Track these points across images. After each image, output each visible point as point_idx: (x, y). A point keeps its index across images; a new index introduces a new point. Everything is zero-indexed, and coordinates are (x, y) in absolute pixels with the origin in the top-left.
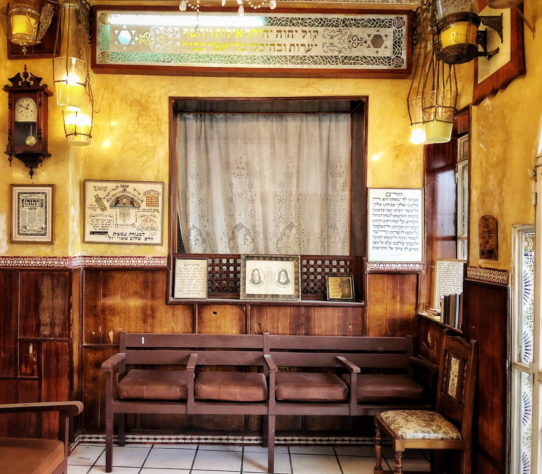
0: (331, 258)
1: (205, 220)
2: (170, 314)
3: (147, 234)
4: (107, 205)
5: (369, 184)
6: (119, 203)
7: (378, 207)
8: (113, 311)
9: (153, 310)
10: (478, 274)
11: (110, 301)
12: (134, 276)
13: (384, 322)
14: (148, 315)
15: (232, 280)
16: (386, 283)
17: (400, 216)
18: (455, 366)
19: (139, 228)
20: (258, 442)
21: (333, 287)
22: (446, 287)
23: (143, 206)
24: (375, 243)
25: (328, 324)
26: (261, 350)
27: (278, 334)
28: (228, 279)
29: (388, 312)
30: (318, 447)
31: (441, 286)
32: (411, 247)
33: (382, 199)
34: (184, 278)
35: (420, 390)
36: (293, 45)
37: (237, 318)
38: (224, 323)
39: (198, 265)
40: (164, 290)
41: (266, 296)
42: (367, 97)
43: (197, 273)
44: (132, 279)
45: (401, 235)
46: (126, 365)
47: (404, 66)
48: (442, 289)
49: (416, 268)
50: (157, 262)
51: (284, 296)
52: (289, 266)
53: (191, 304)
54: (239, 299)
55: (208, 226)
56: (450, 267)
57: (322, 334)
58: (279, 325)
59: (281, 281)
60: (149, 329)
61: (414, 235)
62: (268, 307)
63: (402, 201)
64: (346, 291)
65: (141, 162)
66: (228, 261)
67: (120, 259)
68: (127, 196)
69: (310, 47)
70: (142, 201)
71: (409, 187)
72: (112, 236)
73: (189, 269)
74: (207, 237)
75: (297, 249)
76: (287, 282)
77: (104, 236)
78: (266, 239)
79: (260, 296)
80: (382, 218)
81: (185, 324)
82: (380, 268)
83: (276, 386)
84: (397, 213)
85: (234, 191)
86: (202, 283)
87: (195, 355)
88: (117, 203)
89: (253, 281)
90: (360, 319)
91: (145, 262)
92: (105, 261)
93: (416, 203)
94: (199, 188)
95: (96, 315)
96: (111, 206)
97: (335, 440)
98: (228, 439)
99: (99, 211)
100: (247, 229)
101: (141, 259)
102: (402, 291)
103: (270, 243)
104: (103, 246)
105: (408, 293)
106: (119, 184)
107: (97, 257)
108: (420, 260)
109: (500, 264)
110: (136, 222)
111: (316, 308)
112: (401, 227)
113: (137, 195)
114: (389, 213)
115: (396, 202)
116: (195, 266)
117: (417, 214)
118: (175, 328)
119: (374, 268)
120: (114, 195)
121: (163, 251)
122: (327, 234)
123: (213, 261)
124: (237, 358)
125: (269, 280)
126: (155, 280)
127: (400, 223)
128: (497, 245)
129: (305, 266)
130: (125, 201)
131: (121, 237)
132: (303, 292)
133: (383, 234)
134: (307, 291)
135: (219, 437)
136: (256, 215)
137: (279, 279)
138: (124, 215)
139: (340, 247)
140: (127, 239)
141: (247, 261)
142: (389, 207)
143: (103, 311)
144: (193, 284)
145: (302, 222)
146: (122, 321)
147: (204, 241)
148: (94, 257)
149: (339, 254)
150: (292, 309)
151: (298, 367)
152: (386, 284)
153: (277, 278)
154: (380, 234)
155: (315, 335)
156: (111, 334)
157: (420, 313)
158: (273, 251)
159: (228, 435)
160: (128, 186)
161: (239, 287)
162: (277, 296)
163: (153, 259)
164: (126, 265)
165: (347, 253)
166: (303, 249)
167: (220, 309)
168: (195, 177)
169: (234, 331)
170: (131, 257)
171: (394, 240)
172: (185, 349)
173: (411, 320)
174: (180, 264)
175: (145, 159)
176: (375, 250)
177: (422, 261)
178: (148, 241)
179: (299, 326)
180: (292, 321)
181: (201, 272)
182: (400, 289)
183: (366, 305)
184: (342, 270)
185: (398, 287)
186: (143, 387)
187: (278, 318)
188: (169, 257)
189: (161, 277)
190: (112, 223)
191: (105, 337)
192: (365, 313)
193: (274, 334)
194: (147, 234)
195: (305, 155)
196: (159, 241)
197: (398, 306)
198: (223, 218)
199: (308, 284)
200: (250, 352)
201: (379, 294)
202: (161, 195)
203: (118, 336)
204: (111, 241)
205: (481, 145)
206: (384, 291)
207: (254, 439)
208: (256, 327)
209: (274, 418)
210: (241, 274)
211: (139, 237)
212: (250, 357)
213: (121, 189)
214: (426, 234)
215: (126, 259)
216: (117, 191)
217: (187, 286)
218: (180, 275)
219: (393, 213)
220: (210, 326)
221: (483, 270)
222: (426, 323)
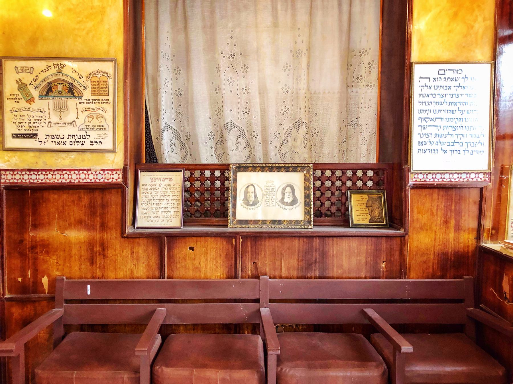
1: (184, 117)
2: (127, 252)
3: (94, 136)
4: (35, 94)
5: (414, 56)
6: (52, 91)
7: (426, 91)
8: (46, 247)
9: (104, 246)
11: (42, 234)
12: (76, 196)
13: (432, 257)
14: (96, 252)
15: (217, 200)
16: (436, 201)
19: (82, 127)
23: (87, 94)
24: (421, 143)
25: (350, 259)
26: (257, 301)
27: (281, 277)
28: (212, 200)
29: (437, 244)
32: (474, 149)
33: (432, 80)
34: (150, 198)
35: (501, 373)
37: (224, 255)
38: (205, 262)
39: (171, 180)
40: (119, 217)
41: (264, 222)
43: (169, 191)
44: (73, 202)
46: (64, 325)
50: (108, 176)
51: (290, 222)
52: (297, 179)
53: (156, 237)
54: (226, 226)
55: (188, 125)
57: (344, 276)
58: (283, 265)
60: (99, 273)
62: (267, 239)
63: (461, 81)
64: (377, 213)
65: (84, 30)
66: (212, 174)
67: (56, 172)
68: (64, 80)
70: (85, 88)
72: (43, 140)
73: (157, 186)
74: (186, 140)
75: (306, 156)
76: (294, 202)
77: (32, 140)
78: (265, 142)
79: (256, 222)
80: (432, 107)
81: (149, 265)
82: (428, 180)
83: (278, 365)
84: (454, 99)
85: (222, 76)
86: (176, 206)
87: (162, 310)
88: (49, 91)
90: (397, 253)
91: (91, 177)
92: (34, 177)
94: (176, 74)
95: (23, 255)
96: (41, 97)
99: (23, 103)
100: (240, 130)
101: (85, 172)
102: (458, 213)
103: (271, 147)
104: (31, 154)
105: (467, 215)
106: (51, 63)
107: (22, 171)
108: (486, 168)
110: (77, 118)
111: (335, 239)
112: (459, 119)
113: (77, 78)
114: (442, 100)
115: (454, 83)
116: (166, 182)
118: (135, 272)
119: (418, 180)
120: (44, 80)
121: (117, 160)
122: (347, 135)
123: (192, 174)
124: (221, 314)
125: (269, 199)
126: (105, 202)
127: (457, 115)
129: (319, 179)
130: (60, 88)
131: (57, 140)
132: (315, 215)
133: (433, 130)
134: (321, 213)
136: (252, 110)
137: (283, 198)
138: (60, 109)
139: (365, 150)
140: (65, 144)
142: (442, 91)
143: (33, 248)
144: (162, 206)
145: (314, 118)
146: (61, 262)
147: (183, 146)
148: (18, 170)
149: (363, 160)
150: (301, 240)
151: (309, 325)
152: (435, 203)
153: (280, 197)
155: (333, 278)
156: (45, 280)
157: (483, 244)
158: (275, 159)
160: (64, 66)
161: (228, 210)
162: (280, 222)
163: (102, 172)
164: (64, 181)
165: (373, 159)
166: (314, 154)
167: (198, 243)
168: (170, 58)
169: (219, 274)
170: (70, 170)
171: (449, 139)
172: (148, 301)
173: (470, 254)
174: (145, 178)
175: (90, 25)
176: (422, 154)
177: (489, 168)
178: (95, 147)
179: (311, 265)
180: (300, 258)
181: (174, 190)
182: (455, 210)
183: (406, 234)
184: (370, 183)
185: (453, 207)
186: (72, 374)
187: (281, 254)
188: (125, 171)
189: (114, 198)
190: (43, 120)
191: (37, 285)
192: (404, 245)
193: (275, 277)
194: (94, 136)
195: (319, 25)
196: (110, 147)
197: (452, 235)
198: (208, 115)
199: (322, 204)
200: (241, 305)
201: (424, 218)
202: (112, 77)
203: (53, 283)
204: (42, 146)
206: (432, 214)
208: (250, 267)
210: (230, 191)
211: (81, 140)
212: (243, 310)
213: (54, 70)
215: (64, 172)
216: (48, 73)
217: (154, 210)
218: (144, 194)
219: (448, 99)
220: (185, 267)
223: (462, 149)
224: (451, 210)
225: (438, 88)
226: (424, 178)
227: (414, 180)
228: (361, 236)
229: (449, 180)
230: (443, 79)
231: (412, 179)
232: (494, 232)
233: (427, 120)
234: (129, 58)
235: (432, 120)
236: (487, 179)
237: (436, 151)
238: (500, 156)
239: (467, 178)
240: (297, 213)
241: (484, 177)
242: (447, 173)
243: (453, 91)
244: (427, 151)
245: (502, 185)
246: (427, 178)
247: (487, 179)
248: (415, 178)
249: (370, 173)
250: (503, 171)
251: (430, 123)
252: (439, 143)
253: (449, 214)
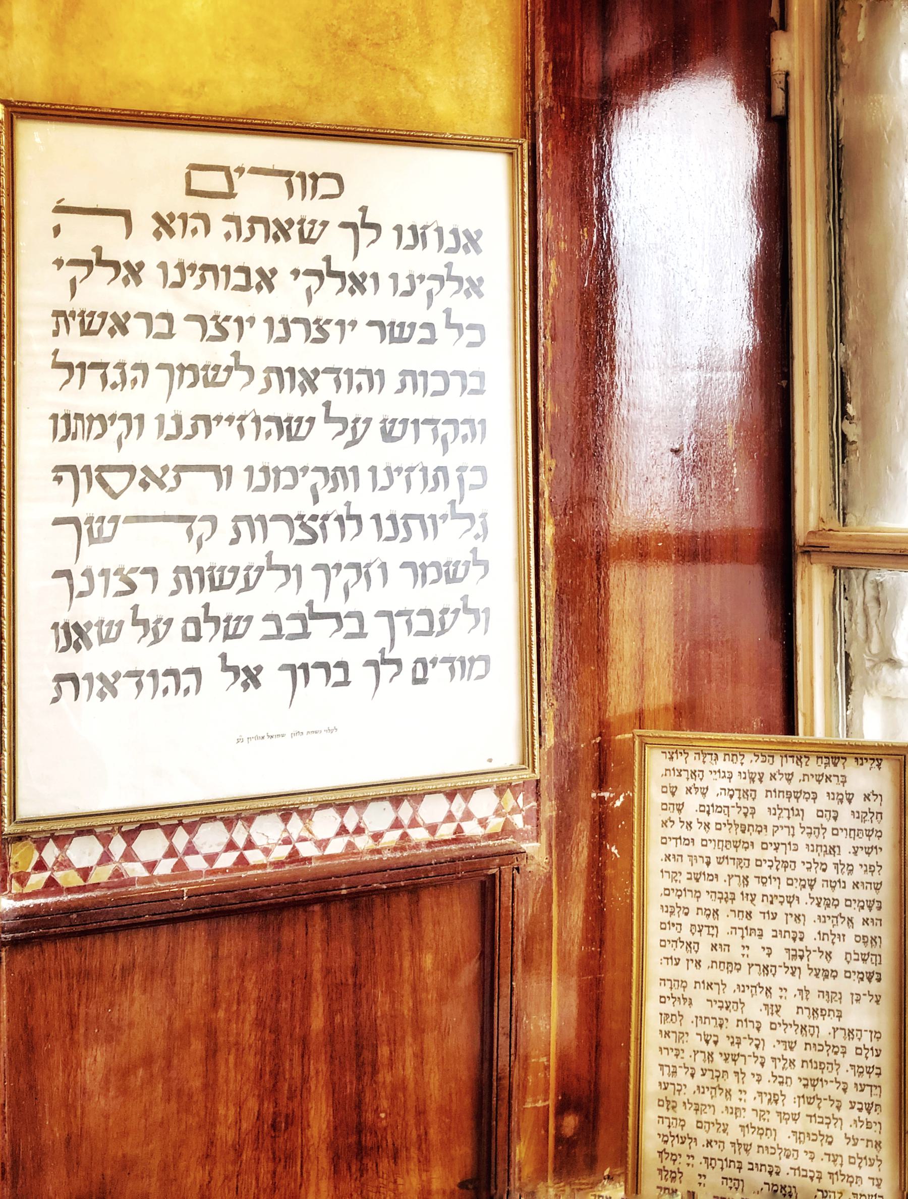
17: (325, 382)
22: (733, 979)
31: (691, 974)
33: (144, 224)
48: (700, 996)
49: (471, 829)
56: (762, 804)
61: (452, 543)
63: (336, 245)
71: (391, 122)
82: (136, 870)
84: (299, 353)
93: (465, 264)
112: (336, 476)
114: (221, 353)
115: (286, 255)
117: (468, 360)
127: (322, 447)
141: (117, 492)
154: (129, 548)
171: (273, 597)
177: (527, 759)
214: (549, 531)
219: (258, 348)
224: (304, 1041)
225: (192, 281)
226: (106, 858)
227: (37, 880)
229: (282, 853)
230: (219, 227)
231: (22, 879)
232: (571, 1122)
233: (116, 480)
234: (806, 62)
235: (149, 479)
236: (518, 820)
237: (188, 681)
239: (397, 824)
241: (498, 813)
242: (211, 818)
243: (287, 299)
244: (126, 686)
246: (129, 856)
247: (518, 820)
248: (40, 866)
251: (136, 500)
252: (207, 629)
253: (292, 1070)
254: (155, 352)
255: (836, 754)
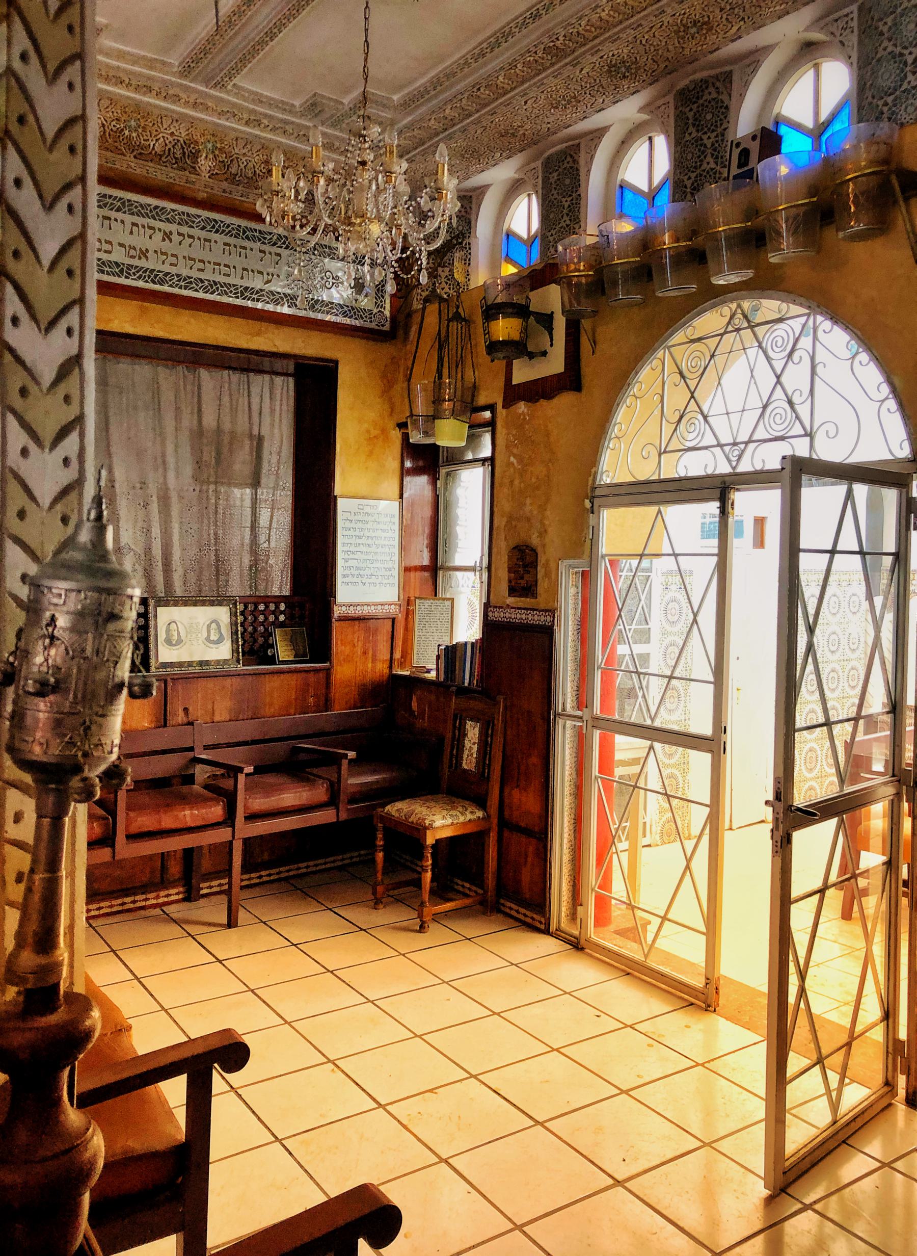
0: (267, 600)
10: (507, 615)
18: (473, 732)
20: (181, 896)
21: (284, 644)
24: (344, 576)
26: (191, 749)
30: (268, 886)
36: (246, 270)
41: (190, 664)
42: (336, 362)
45: (375, 565)
47: (387, 327)
51: (218, 662)
52: (222, 614)
59: (212, 638)
69: (270, 277)
76: (220, 640)
89: (169, 641)
97: (288, 871)
98: (134, 902)
102: (375, 643)
109: (542, 600)
128: (536, 581)
135: (120, 901)
137: (209, 636)
141: (158, 609)
152: (356, 636)
153: (205, 635)
157: (394, 672)
159: (135, 894)
162: (207, 663)
165: (286, 592)
171: (367, 572)
177: (399, 599)
184: (282, 618)
205: (512, 459)
207: (175, 893)
209: (241, 842)
221: (515, 611)
222: (415, 683)
223: (378, 581)
228: (393, 632)
235: (353, 553)
238: (407, 589)
240: (223, 651)
245: (409, 614)
249: (282, 607)
250: (409, 603)
251: (352, 556)
254: (354, 534)
255: (444, 599)
